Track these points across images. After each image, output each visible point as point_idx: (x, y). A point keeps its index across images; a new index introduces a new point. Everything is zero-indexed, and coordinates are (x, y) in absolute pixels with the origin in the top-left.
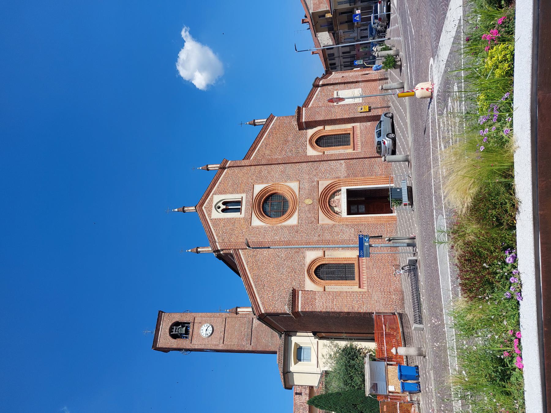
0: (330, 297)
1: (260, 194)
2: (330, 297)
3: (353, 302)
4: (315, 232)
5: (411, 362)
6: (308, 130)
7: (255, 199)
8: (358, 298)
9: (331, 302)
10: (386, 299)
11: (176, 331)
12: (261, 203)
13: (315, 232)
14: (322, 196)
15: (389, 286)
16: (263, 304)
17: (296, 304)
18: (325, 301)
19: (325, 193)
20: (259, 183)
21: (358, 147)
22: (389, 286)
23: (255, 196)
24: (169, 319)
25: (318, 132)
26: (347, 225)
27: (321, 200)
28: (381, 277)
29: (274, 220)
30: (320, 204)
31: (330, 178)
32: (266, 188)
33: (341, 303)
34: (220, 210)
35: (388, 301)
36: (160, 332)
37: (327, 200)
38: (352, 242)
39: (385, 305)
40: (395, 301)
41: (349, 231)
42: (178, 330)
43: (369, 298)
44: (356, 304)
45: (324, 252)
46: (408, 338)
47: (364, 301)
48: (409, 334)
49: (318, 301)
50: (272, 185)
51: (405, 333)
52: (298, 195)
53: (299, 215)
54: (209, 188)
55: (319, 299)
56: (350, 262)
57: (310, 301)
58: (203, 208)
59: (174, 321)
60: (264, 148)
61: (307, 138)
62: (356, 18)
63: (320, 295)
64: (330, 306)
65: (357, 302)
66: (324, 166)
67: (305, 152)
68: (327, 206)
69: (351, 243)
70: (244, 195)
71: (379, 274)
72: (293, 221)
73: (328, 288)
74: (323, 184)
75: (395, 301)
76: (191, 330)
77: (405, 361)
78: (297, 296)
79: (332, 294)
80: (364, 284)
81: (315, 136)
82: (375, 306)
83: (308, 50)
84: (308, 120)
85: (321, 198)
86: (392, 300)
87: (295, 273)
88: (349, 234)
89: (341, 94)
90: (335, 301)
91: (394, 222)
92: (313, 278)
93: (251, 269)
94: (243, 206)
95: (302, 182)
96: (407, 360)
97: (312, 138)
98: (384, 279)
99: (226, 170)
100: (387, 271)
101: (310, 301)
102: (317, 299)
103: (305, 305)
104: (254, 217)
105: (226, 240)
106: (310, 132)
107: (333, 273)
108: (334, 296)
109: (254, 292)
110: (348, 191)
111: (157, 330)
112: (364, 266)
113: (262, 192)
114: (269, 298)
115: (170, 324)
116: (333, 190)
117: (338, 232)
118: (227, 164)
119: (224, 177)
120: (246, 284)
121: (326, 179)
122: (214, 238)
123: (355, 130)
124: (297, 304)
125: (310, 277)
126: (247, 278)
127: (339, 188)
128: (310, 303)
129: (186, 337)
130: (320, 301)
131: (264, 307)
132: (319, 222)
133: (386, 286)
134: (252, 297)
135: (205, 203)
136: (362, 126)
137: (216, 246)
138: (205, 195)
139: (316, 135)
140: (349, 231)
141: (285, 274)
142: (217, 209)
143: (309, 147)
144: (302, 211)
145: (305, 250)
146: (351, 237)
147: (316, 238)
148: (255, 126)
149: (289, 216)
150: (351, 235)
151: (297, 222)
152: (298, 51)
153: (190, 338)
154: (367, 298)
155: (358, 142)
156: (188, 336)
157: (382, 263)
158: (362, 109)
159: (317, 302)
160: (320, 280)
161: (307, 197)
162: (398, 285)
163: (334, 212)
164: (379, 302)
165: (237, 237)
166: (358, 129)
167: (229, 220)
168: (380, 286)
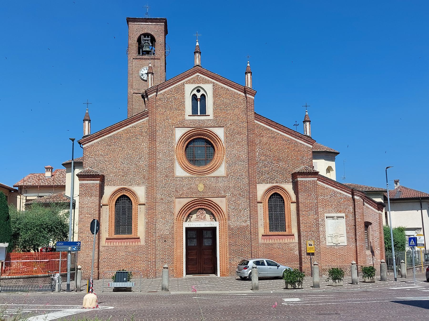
0: (92, 210)
1: (212, 135)
2: (93, 211)
3: (88, 233)
4: (167, 194)
5: (5, 282)
6: (292, 184)
7: (207, 130)
8: (91, 237)
9: (88, 212)
10: (90, 263)
11: (146, 40)
12: (203, 137)
13: (167, 194)
14: (208, 201)
15: (108, 267)
16: (92, 145)
17: (86, 179)
18: (89, 206)
19: (211, 205)
20: (225, 133)
21: (267, 240)
22: (107, 267)
23: (211, 129)
24: (157, 31)
25: (289, 196)
26: (173, 227)
27: (203, 200)
28: (117, 260)
29: (181, 152)
30: (198, 199)
31: (228, 210)
32: (220, 141)
33: (87, 221)
34: (195, 92)
35: (88, 265)
36: (144, 23)
37: (203, 207)
38: (153, 233)
39: (85, 263)
40: (88, 272)
41: (166, 229)
42: (147, 43)
43: (91, 248)
44: (86, 235)
45: (145, 205)
46: (30, 281)
47: (89, 243)
48: (35, 282)
49: (89, 199)
50: (223, 147)
51: (37, 278)
52: (209, 175)
53: (186, 178)
54: (221, 78)
55: (91, 200)
56: (133, 230)
57: (88, 192)
58: (198, 73)
59: (156, 37)
60: (270, 135)
61: (282, 183)
62: (412, 241)
63: (95, 201)
64: (84, 210)
65: (87, 236)
66: (243, 202)
67: (263, 181)
68: (197, 206)
69: (152, 231)
70: (211, 117)
71: (120, 258)
72: (180, 172)
73: (106, 209)
74: (221, 202)
75: (88, 272)
76: (146, 56)
77: (6, 277)
78: (94, 179)
79: (95, 213)
80: (111, 243)
81: (283, 192)
82: (84, 253)
83: (387, 182)
84: (299, 184)
85: (201, 200)
86: (89, 269)
87: (123, 176)
88: (163, 229)
89: (339, 221)
90: (88, 216)
91: (174, 275)
92: (117, 194)
93: (128, 131)
94: (198, 118)
95: (225, 180)
96: (7, 279)
97: (281, 189)
98: (115, 263)
99: (244, 94)
100: (123, 265)
101: (88, 192)
102: (91, 198)
103: (85, 187)
104: (184, 130)
105: (159, 103)
106: (289, 187)
107: (124, 214)
108: (93, 214)
109: (103, 136)
110: (214, 229)
111: (146, 20)
112: (128, 244)
113: (215, 137)
114: (98, 151)
115: (152, 33)
116: (216, 213)
117: (166, 218)
118: (251, 95)
119: (235, 93)
120: (111, 128)
121: (228, 205)
122: (161, 90)
123: (289, 237)
124: (86, 180)
125: (118, 190)
126: (118, 128)
127: (217, 219)
128: (87, 192)
129: (139, 53)
130: (89, 201)
131: (88, 147)
132: (177, 199)
133: (108, 264)
134: (98, 134)
135: (203, 76)
136: (294, 244)
137: (152, 93)
138: (213, 74)
139: (284, 193)
140: (166, 229)
141: (121, 166)
142: (196, 90)
143: (269, 186)
144: (191, 181)
145: (146, 185)
146: (159, 231)
147: (159, 196)
148: (303, 122)
149: (185, 167)
150: (162, 231)
151: (178, 176)
152: (386, 170)
153: (140, 57)
154: (92, 246)
155: (273, 240)
156: (141, 55)
157: (132, 261)
158: (310, 245)
159: (88, 198)
160: (116, 201)
161: (207, 185)
162: (109, 275)
163: (190, 214)
164: (88, 257)
165: (163, 114)
166: (290, 240)
167: (183, 103)
168: (108, 258)
